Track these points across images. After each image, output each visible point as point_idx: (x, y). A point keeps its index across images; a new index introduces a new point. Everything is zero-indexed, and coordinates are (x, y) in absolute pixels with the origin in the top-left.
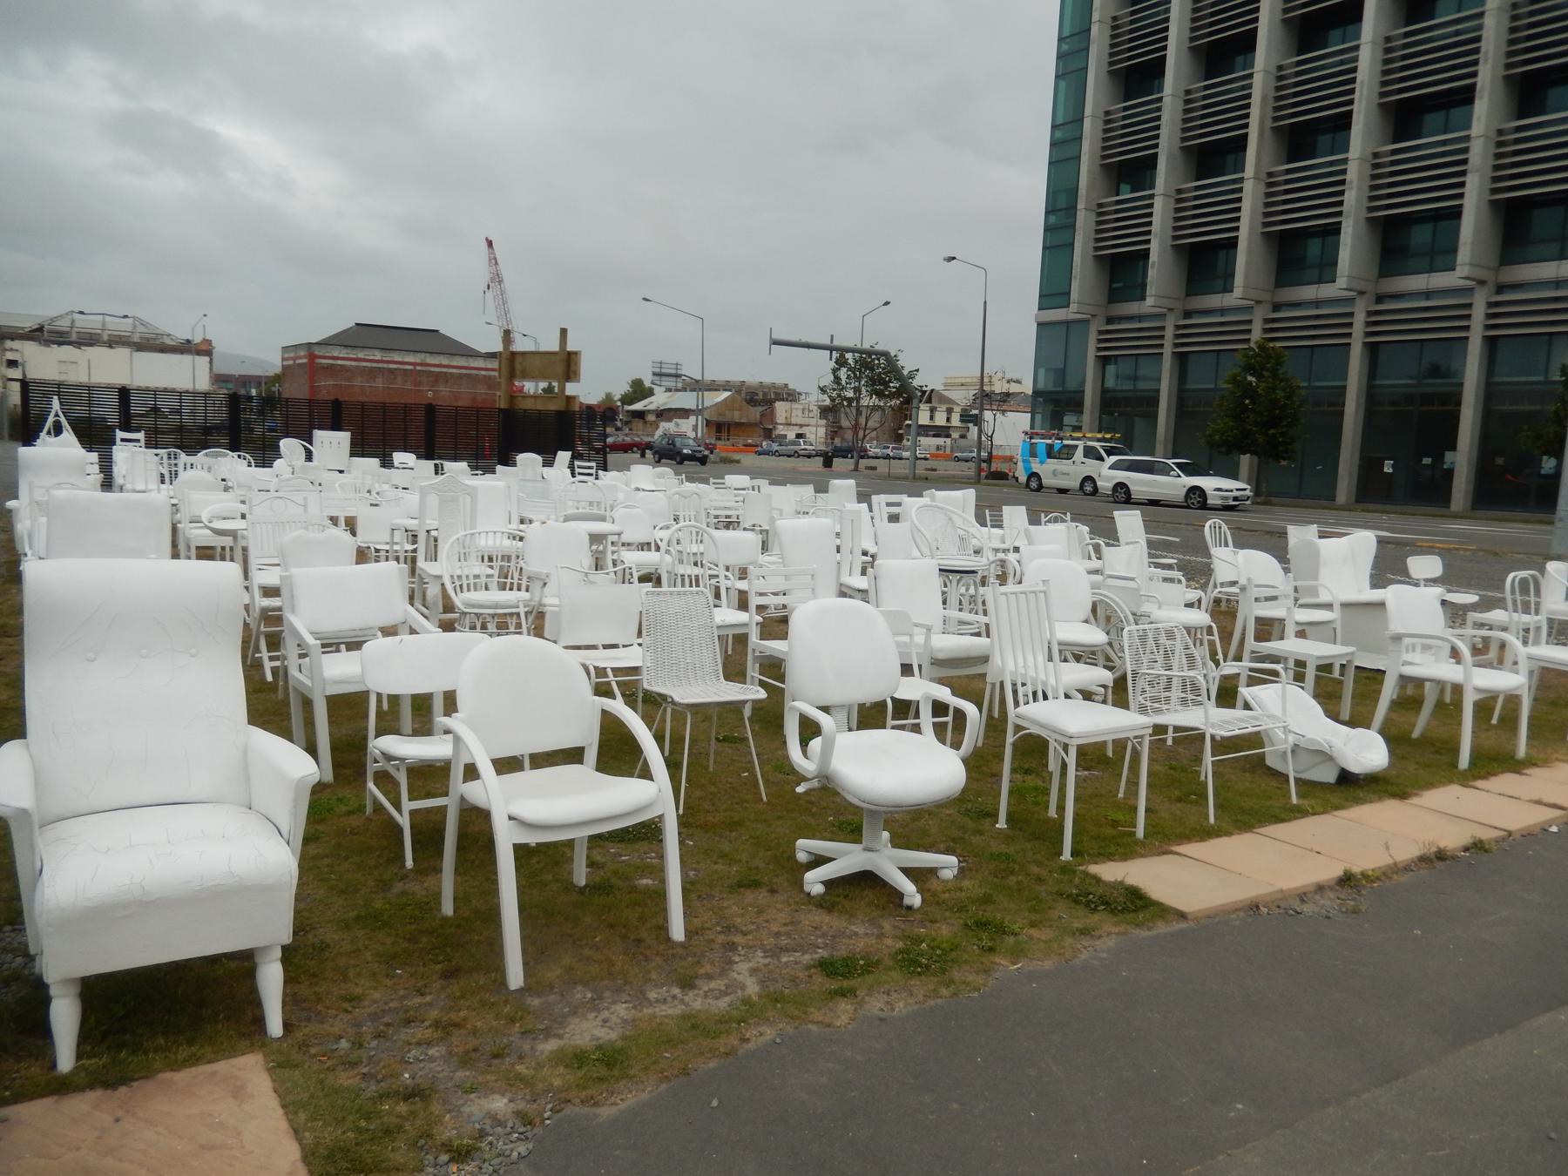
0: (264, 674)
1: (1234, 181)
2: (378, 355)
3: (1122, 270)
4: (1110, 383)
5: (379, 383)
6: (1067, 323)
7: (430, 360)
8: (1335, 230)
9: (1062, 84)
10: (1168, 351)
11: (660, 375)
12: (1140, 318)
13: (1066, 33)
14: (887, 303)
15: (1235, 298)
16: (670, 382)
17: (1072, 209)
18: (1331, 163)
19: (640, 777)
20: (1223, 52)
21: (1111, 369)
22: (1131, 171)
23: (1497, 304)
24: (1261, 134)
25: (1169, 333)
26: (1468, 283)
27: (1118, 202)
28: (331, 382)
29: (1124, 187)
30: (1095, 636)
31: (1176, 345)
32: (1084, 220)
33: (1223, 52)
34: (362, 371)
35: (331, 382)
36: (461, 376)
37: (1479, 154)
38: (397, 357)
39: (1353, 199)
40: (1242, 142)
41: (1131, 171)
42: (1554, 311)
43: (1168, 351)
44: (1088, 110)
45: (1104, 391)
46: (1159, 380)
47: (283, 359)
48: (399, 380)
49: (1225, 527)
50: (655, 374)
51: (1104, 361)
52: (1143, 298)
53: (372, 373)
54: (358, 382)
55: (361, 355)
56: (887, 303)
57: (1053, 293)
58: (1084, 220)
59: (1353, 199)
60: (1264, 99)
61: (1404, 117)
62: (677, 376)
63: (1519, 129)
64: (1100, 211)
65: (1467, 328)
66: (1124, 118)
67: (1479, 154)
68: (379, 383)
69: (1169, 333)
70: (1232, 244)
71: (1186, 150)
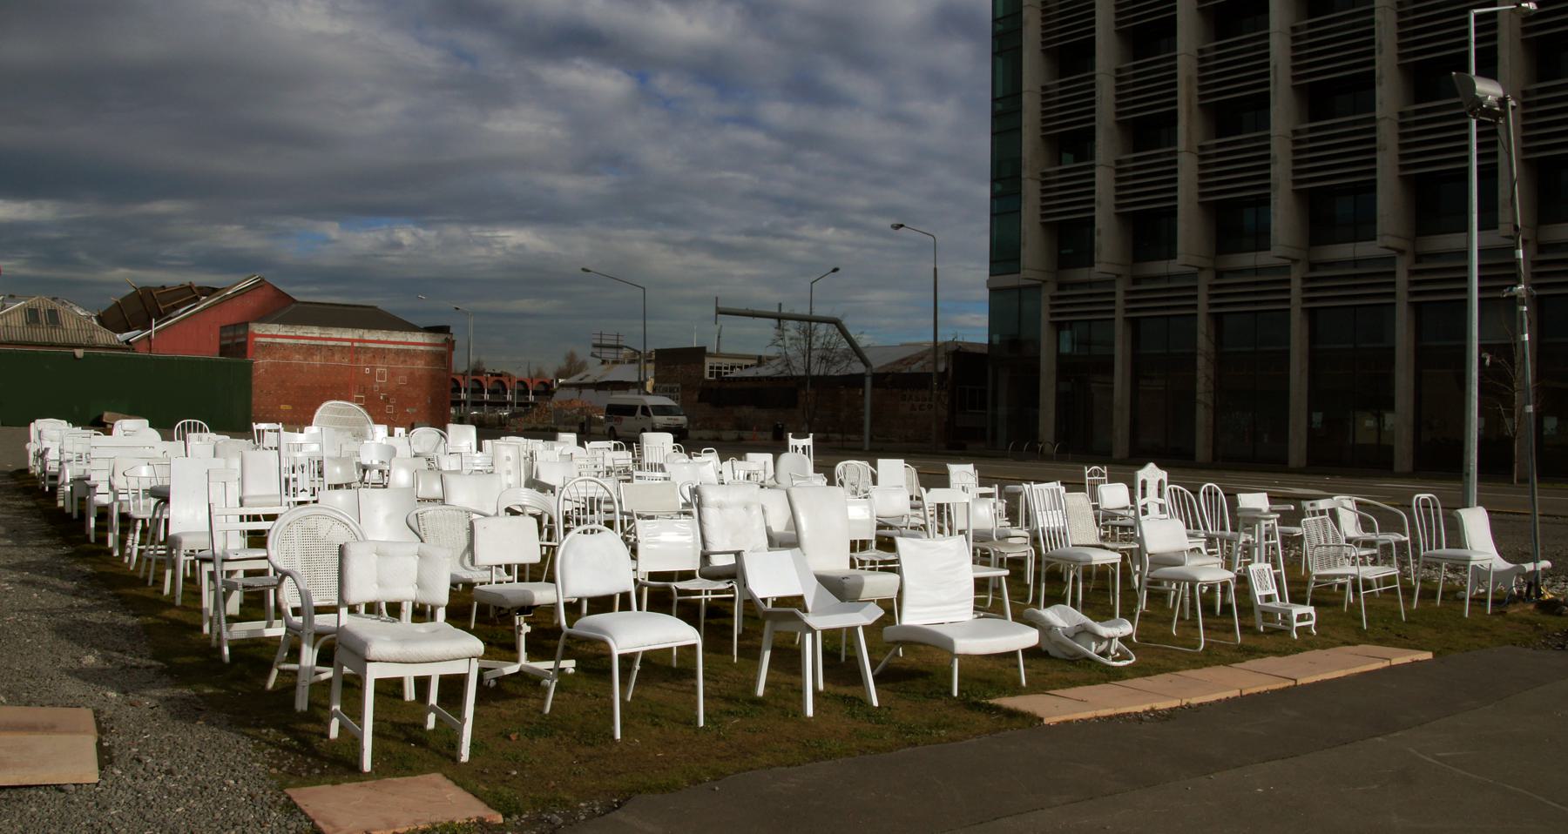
0: (703, 372)
1: (1170, 154)
2: (316, 332)
3: (1070, 239)
4: (1066, 348)
5: (317, 361)
6: (1019, 288)
7: (369, 335)
8: (1265, 201)
9: (1000, 60)
10: (1119, 316)
11: (601, 346)
12: (1090, 284)
13: (1000, 14)
14: (835, 270)
15: (1174, 266)
16: (610, 355)
17: (1016, 178)
18: (1256, 139)
19: (635, 655)
20: (1148, 36)
21: (1066, 335)
22: (1071, 141)
23: (1312, 280)
24: (1189, 112)
25: (1120, 298)
26: (1287, 262)
27: (1061, 172)
28: (269, 360)
29: (1067, 157)
30: (600, 184)
31: (1127, 311)
32: (1031, 191)
33: (1148, 36)
34: (298, 349)
35: (269, 360)
36: (398, 352)
37: (1387, 135)
38: (335, 333)
39: (1281, 171)
40: (1172, 118)
41: (1071, 141)
42: (1168, 299)
43: (1119, 316)
44: (1026, 85)
45: (1059, 356)
46: (1112, 345)
47: (221, 338)
48: (337, 357)
49: (1221, 493)
50: (595, 346)
51: (1059, 327)
52: (1092, 264)
53: (310, 350)
54: (297, 359)
55: (299, 333)
56: (835, 270)
57: (1004, 255)
58: (1031, 191)
59: (1281, 171)
60: (1189, 79)
61: (1318, 98)
62: (619, 347)
63: (1418, 112)
64: (1045, 179)
65: (1113, 311)
66: (1061, 93)
67: (1387, 135)
68: (317, 361)
69: (1120, 298)
70: (1173, 212)
71: (1121, 124)
